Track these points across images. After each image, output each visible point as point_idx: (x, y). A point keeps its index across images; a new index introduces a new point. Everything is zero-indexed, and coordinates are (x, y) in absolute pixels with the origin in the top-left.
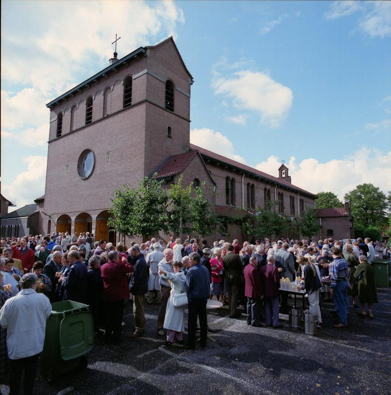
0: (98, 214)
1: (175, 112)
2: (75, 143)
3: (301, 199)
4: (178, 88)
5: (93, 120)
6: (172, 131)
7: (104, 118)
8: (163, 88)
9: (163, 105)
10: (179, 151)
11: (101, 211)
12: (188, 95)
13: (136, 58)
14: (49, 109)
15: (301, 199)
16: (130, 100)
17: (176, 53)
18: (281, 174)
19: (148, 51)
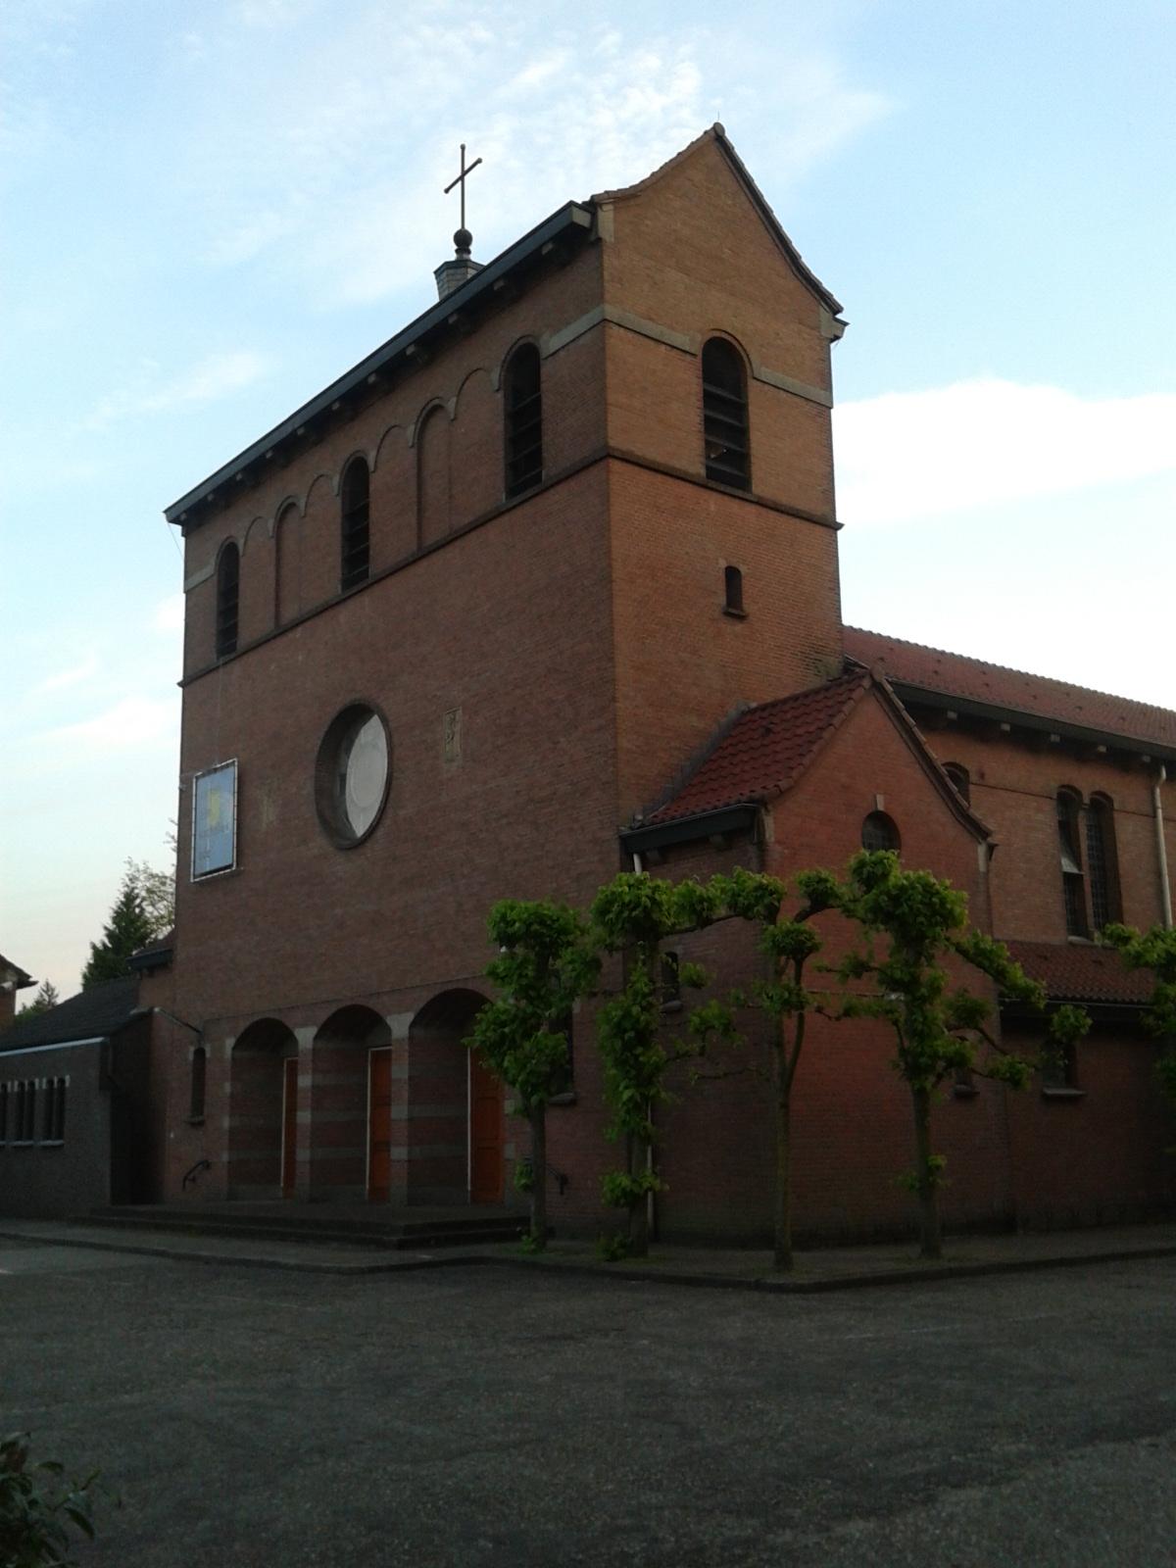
1: (758, 488)
5: (375, 568)
6: (748, 586)
8: (689, 380)
9: (693, 461)
10: (778, 676)
12: (814, 392)
14: (178, 529)
16: (535, 458)
17: (743, 199)
19: (606, 215)
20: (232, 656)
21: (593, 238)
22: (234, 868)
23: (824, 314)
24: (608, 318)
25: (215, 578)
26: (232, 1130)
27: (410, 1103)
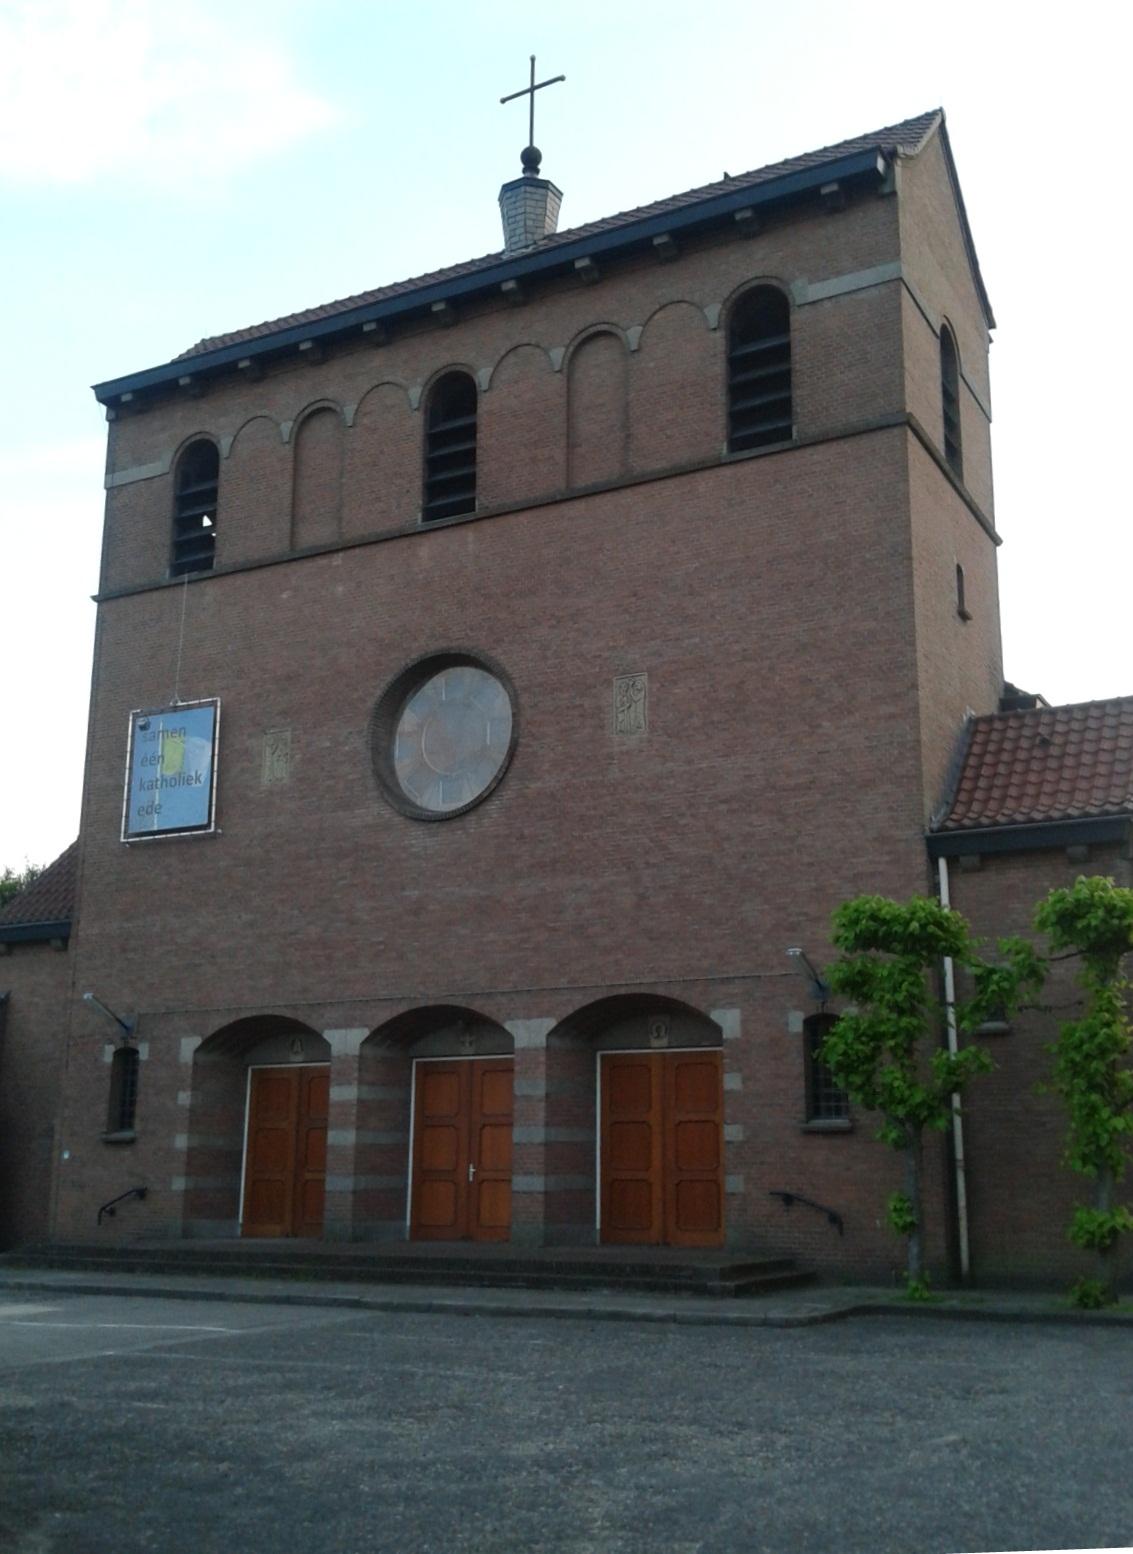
11: (580, 1001)
20: (206, 574)
21: (886, 189)
22: (212, 829)
23: (984, 323)
24: (906, 279)
25: (170, 478)
26: (191, 1151)
27: (547, 1124)
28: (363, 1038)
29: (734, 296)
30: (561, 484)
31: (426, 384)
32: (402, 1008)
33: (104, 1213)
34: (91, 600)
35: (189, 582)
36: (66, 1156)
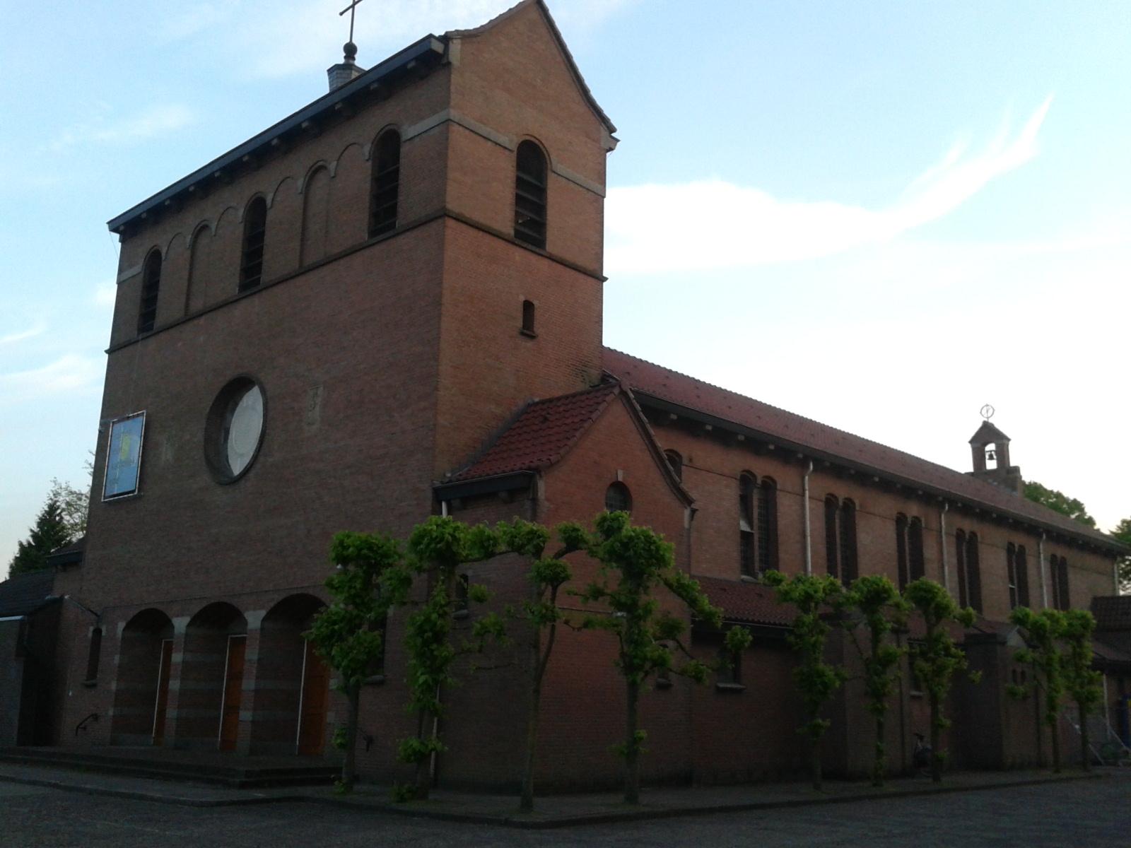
0: (272, 604)
1: (550, 247)
2: (204, 350)
3: (1054, 557)
4: (560, 164)
6: (538, 314)
7: (303, 271)
8: (506, 168)
11: (278, 597)
12: (595, 186)
13: (305, 130)
14: (117, 236)
15: (1054, 557)
16: (392, 211)
18: (979, 458)
19: (455, 47)
21: (444, 61)
22: (136, 493)
24: (452, 118)
27: (257, 678)
28: (186, 624)
29: (381, 133)
30: (301, 266)
31: (246, 206)
32: (205, 604)
33: (79, 730)
34: (105, 353)
35: (142, 339)
36: (70, 694)
